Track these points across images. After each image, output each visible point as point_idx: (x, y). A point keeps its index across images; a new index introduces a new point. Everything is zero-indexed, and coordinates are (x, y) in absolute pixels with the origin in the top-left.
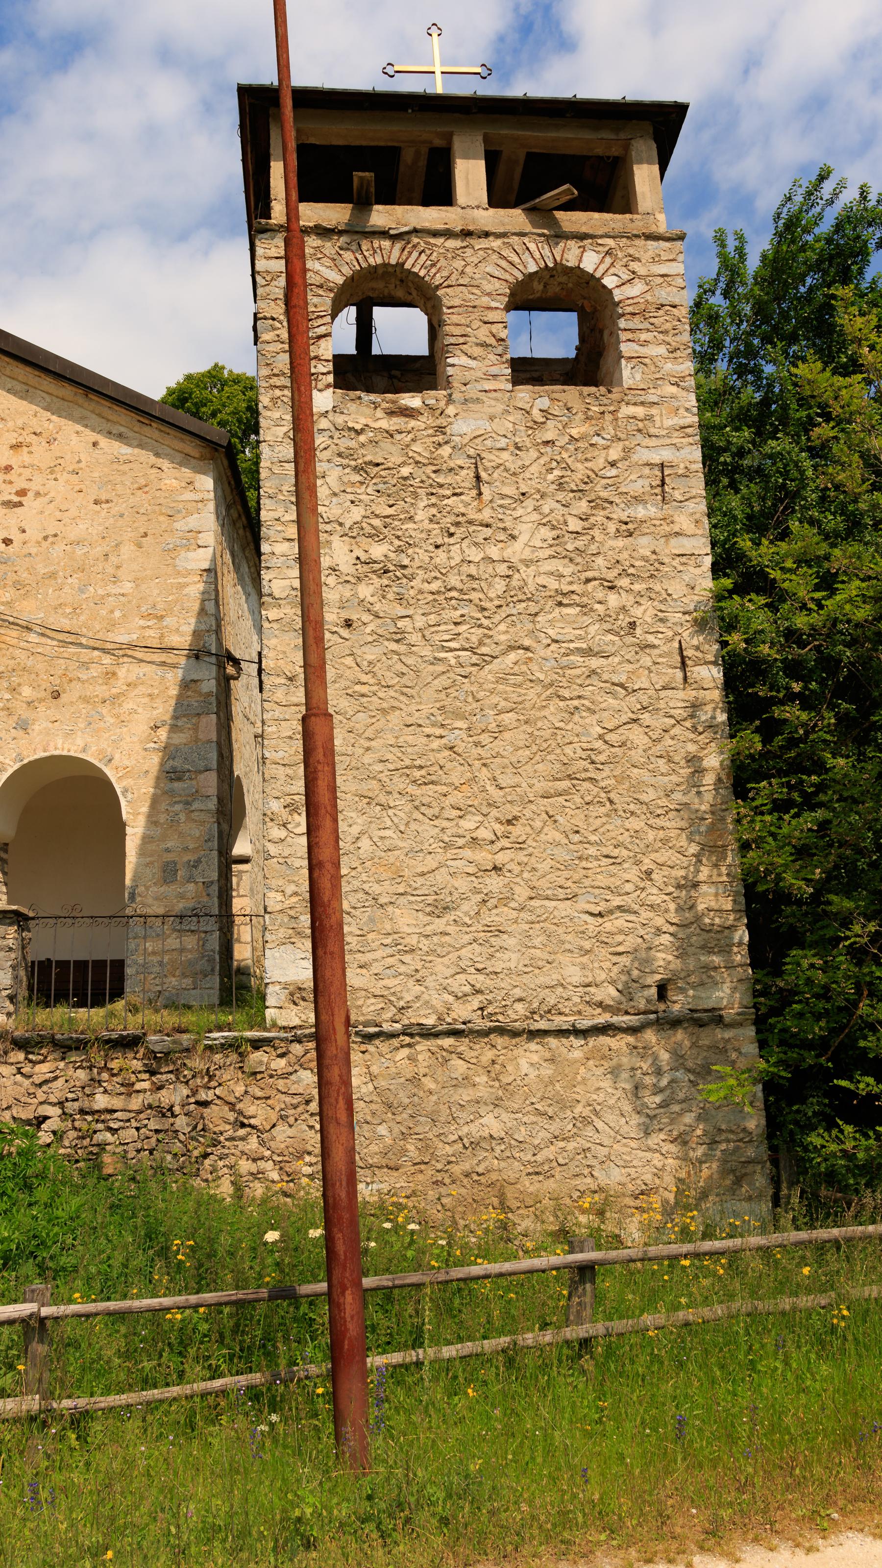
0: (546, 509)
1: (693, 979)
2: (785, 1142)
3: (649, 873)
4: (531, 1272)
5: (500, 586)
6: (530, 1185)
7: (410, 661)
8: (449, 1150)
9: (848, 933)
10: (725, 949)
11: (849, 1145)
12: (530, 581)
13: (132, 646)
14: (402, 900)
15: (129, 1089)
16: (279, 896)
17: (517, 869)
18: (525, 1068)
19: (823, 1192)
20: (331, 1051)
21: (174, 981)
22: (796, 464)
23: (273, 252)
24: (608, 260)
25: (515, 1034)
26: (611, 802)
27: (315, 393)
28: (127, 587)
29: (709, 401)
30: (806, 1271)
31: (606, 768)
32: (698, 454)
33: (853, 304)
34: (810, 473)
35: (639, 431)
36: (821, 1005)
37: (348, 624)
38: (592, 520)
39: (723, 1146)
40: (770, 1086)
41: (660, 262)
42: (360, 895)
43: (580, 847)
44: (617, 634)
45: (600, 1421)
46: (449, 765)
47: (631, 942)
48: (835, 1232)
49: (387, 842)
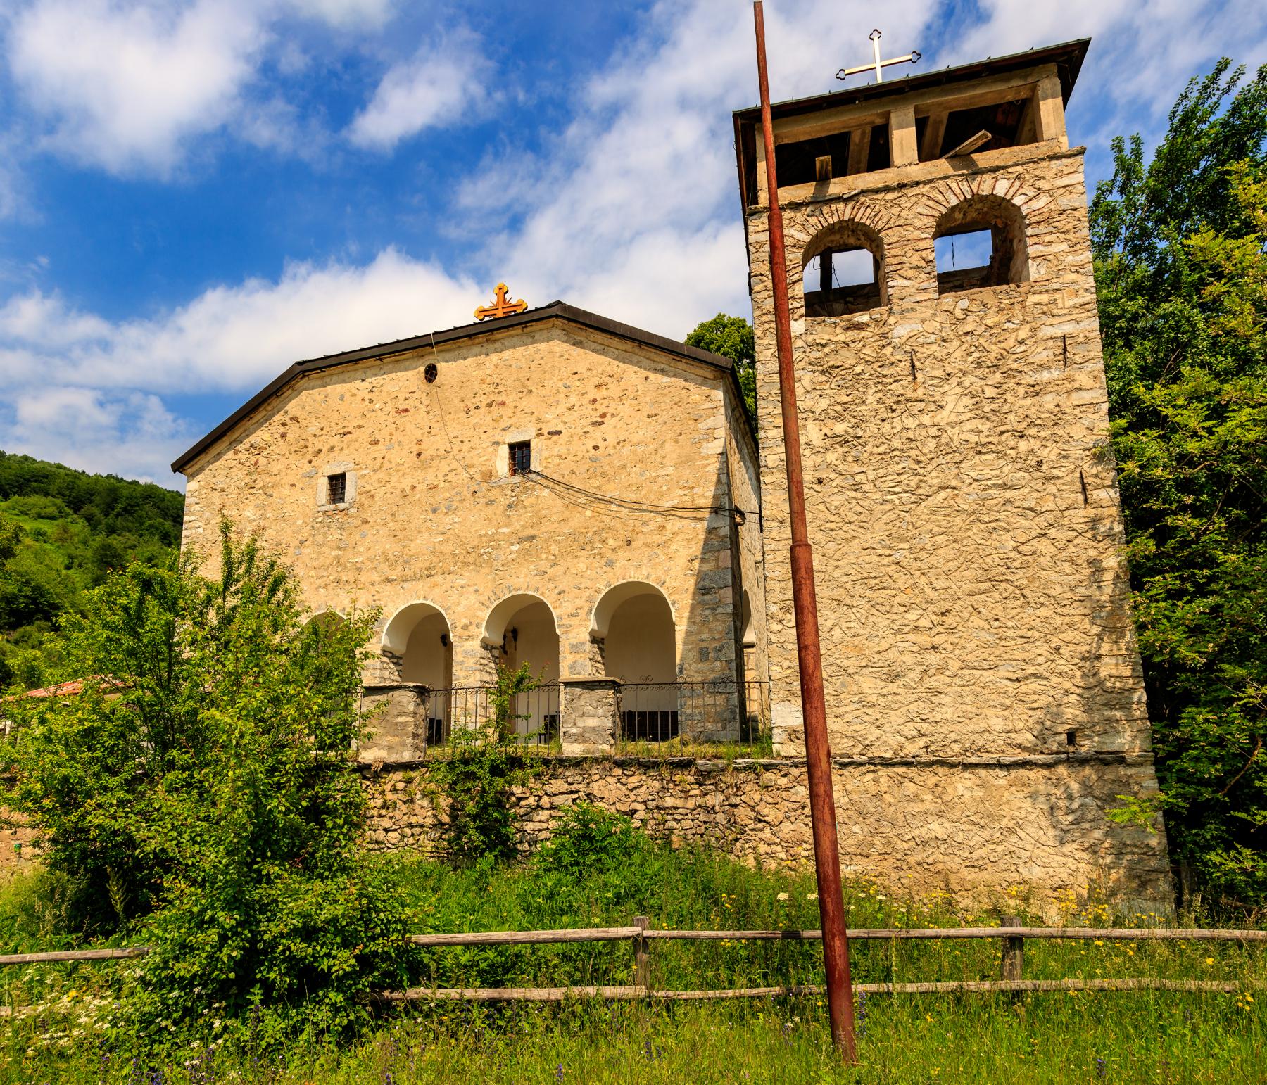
0: (967, 383)
1: (1097, 728)
2: (1185, 857)
3: (1057, 649)
4: (972, 937)
5: (932, 444)
6: (969, 875)
7: (865, 503)
8: (906, 846)
9: (1241, 695)
10: (1126, 706)
11: (1247, 865)
12: (955, 438)
13: (674, 508)
14: (865, 671)
15: (686, 794)
16: (779, 669)
17: (950, 648)
18: (961, 790)
19: (1224, 900)
20: (818, 773)
21: (709, 725)
22: (1188, 320)
23: (761, 228)
24: (1017, 183)
25: (952, 766)
26: (1024, 596)
27: (792, 322)
28: (670, 470)
29: (1106, 280)
30: (1210, 961)
31: (1020, 572)
32: (1095, 324)
33: (1247, 175)
34: (1201, 325)
35: (1044, 313)
36: (1216, 752)
37: (820, 481)
38: (1005, 387)
39: (1129, 857)
40: (1170, 813)
41: (1062, 176)
42: (835, 668)
43: (1000, 630)
44: (1027, 471)
45: (1031, 1053)
46: (896, 575)
47: (1043, 700)
48: (1237, 933)
49: (853, 631)
